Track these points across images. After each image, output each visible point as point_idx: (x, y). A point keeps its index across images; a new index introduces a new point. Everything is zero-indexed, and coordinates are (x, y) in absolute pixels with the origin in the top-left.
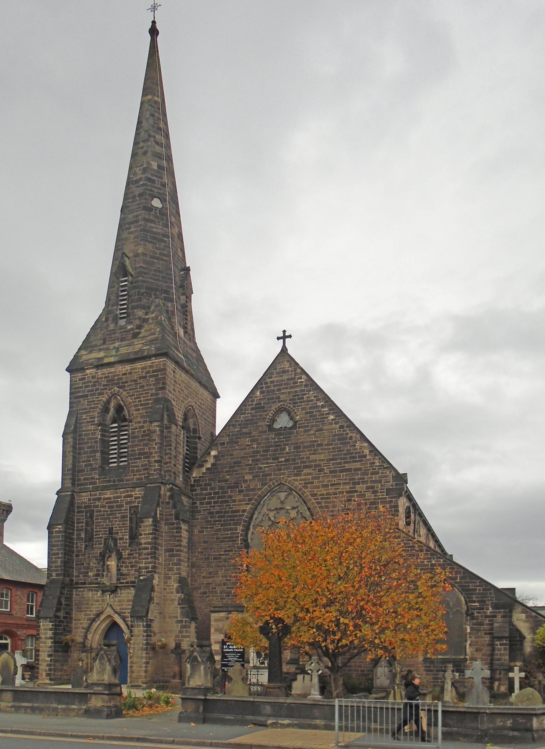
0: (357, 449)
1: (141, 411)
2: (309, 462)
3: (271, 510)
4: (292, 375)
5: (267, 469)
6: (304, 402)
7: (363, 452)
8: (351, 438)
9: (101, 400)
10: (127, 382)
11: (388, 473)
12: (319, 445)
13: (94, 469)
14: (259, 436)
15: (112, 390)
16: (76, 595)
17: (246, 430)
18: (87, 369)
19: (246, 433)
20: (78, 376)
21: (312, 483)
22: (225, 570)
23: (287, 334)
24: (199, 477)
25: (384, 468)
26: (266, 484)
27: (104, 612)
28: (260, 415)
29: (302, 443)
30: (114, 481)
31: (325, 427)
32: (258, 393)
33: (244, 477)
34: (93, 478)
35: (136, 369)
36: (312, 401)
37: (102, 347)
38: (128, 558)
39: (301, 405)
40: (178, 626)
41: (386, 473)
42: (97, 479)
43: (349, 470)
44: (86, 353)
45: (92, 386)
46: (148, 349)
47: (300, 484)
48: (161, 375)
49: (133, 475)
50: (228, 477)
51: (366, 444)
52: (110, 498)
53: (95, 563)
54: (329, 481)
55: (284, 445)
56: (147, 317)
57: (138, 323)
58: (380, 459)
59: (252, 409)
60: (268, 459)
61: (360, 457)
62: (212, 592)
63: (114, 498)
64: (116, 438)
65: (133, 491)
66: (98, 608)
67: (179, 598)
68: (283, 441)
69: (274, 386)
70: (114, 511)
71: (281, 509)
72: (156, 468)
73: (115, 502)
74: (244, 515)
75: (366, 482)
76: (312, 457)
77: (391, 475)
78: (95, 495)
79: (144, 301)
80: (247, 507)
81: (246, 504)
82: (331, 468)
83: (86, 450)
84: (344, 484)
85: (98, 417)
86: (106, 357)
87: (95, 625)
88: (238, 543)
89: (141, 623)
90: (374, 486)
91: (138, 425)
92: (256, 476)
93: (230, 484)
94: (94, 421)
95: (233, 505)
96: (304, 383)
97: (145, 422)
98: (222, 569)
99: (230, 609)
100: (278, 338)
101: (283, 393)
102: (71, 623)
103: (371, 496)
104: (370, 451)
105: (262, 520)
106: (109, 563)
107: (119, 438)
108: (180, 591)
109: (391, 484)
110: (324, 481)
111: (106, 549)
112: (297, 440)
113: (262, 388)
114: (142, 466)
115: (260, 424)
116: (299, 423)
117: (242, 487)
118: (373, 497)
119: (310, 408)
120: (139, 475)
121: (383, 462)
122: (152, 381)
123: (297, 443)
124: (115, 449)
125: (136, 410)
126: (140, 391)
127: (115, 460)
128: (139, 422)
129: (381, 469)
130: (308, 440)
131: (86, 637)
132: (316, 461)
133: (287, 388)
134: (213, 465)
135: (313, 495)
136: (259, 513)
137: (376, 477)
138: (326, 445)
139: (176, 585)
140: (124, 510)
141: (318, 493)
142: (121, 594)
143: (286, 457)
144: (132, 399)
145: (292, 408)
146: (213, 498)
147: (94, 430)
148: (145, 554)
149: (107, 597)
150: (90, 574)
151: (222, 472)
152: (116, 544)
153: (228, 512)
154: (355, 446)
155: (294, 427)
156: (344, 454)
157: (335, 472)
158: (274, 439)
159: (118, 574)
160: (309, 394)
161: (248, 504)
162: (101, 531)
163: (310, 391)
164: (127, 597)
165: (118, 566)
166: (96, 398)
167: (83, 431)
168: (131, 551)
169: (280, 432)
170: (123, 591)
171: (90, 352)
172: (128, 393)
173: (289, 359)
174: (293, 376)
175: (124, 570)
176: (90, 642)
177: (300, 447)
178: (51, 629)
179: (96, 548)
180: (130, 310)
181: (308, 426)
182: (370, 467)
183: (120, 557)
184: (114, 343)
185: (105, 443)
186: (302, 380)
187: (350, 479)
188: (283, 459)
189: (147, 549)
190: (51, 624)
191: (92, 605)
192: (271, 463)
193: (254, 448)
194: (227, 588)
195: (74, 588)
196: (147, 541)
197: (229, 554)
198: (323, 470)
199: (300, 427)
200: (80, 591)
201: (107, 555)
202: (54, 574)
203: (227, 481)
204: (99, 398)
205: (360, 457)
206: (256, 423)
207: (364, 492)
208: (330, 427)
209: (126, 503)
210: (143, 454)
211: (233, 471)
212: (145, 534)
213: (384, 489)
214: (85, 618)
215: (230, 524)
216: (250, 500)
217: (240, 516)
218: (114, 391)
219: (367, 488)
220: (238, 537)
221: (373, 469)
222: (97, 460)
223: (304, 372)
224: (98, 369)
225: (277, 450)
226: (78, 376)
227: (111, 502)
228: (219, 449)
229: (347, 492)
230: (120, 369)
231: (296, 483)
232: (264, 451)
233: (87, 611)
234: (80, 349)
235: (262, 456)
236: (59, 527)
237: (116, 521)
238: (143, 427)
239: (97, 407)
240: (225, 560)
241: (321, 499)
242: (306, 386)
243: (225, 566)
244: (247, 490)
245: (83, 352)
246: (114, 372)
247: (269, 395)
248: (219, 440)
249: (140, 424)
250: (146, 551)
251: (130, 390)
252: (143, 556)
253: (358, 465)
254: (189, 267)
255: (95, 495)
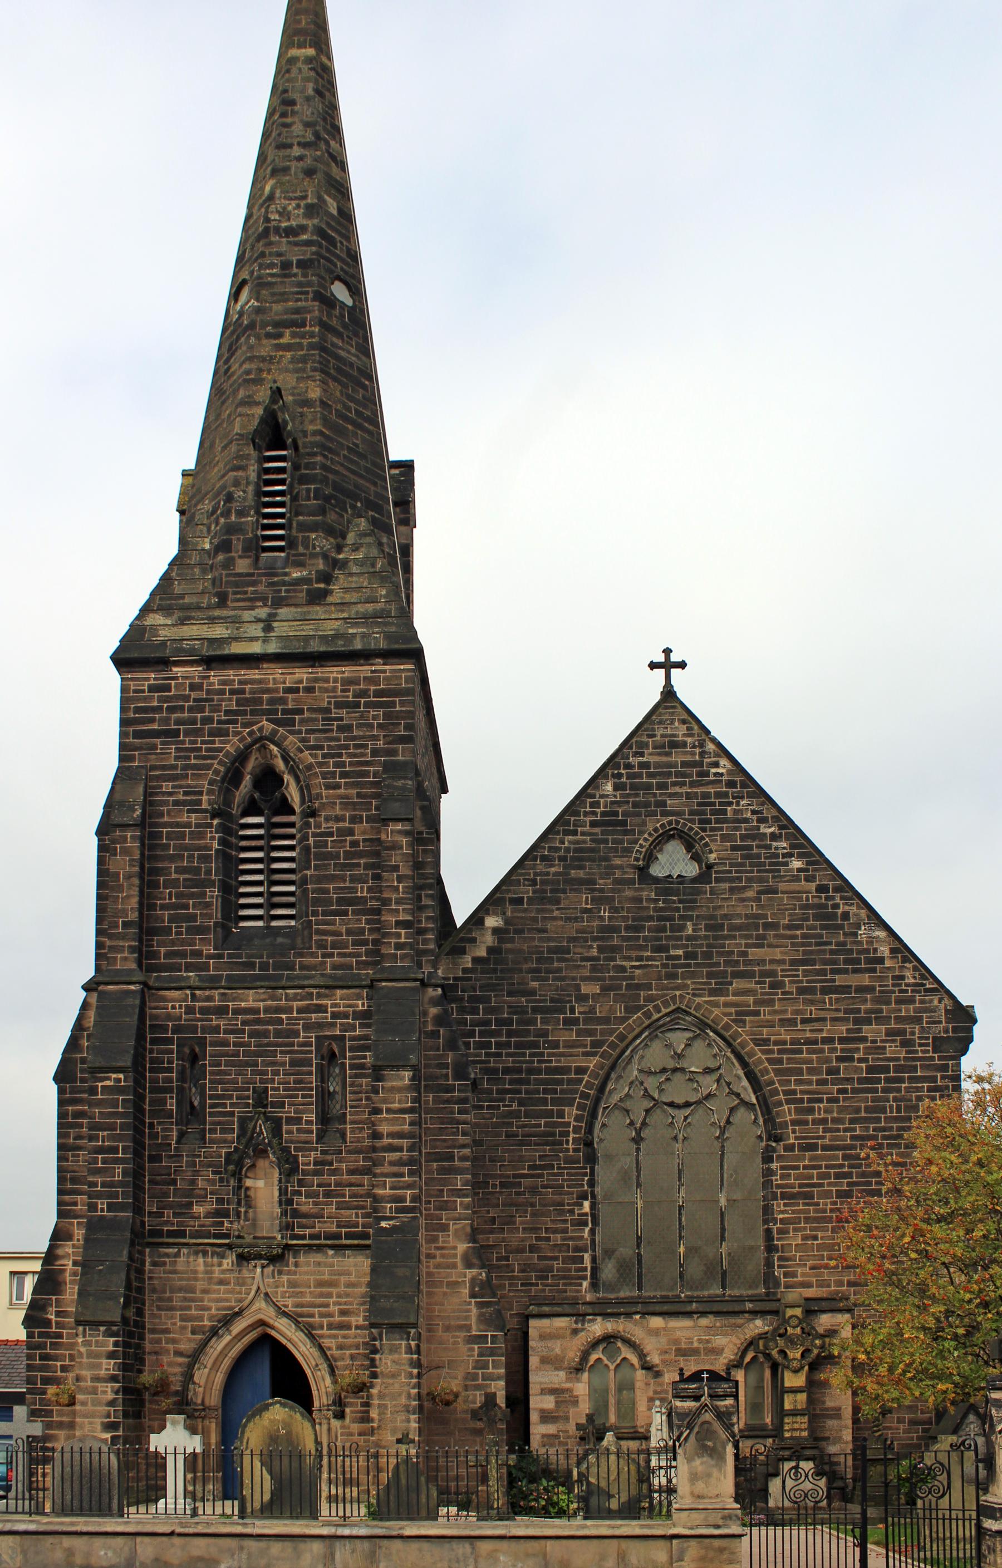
0: (860, 943)
1: (342, 791)
2: (747, 963)
3: (650, 1073)
4: (693, 754)
5: (638, 972)
6: (725, 821)
7: (875, 950)
8: (846, 916)
9: (220, 750)
10: (300, 711)
11: (936, 1002)
12: (767, 926)
13: (202, 930)
14: (613, 890)
15: (254, 728)
16: (154, 1264)
17: (581, 874)
18: (177, 664)
19: (581, 882)
20: (148, 679)
21: (757, 1013)
22: (533, 1215)
23: (674, 658)
24: (455, 979)
25: (926, 990)
26: (639, 1008)
27: (246, 1313)
28: (614, 841)
29: (725, 917)
30: (264, 966)
31: (782, 886)
32: (609, 787)
33: (578, 988)
34: (198, 954)
35: (327, 680)
36: (746, 821)
37: (217, 613)
38: (316, 1173)
39: (721, 829)
40: (472, 1349)
41: (931, 1001)
42: (210, 957)
43: (845, 989)
44: (169, 622)
45: (191, 709)
46: (364, 636)
47: (725, 1014)
48: (402, 704)
49: (324, 956)
50: (535, 984)
51: (882, 934)
52: (256, 1011)
53: (212, 1182)
54: (797, 1012)
55: (682, 918)
56: (341, 556)
57: (321, 567)
58: (915, 969)
59: (593, 824)
60: (641, 948)
61: (868, 961)
62: (499, 1267)
63: (267, 1010)
64: (260, 855)
65: (326, 996)
66: (227, 1300)
67: (473, 1281)
68: (678, 909)
69: (651, 775)
70: (268, 1045)
71: (675, 1070)
72: (403, 940)
73: (271, 1021)
74: (581, 1080)
75: (887, 1020)
76: (754, 953)
77: (942, 1006)
78: (209, 999)
79: (331, 517)
80: (590, 1062)
81: (586, 1054)
82: (801, 982)
83: (174, 876)
84: (834, 1020)
85: (210, 792)
86: (236, 639)
87: (218, 1345)
88: (568, 1150)
89: (404, 1343)
90: (905, 1030)
91: (335, 826)
92: (610, 988)
93: (539, 1001)
94: (199, 802)
95: (549, 1054)
96: (724, 778)
97: (354, 819)
98: (526, 1211)
99: (582, 1309)
100: (653, 666)
101: (672, 795)
102: (142, 1337)
103: (899, 1052)
104: (893, 951)
105: (627, 1095)
106: (249, 1183)
107: (268, 854)
108: (475, 1261)
109: (943, 1027)
110: (785, 1011)
111: (247, 1146)
112: (715, 908)
113: (619, 776)
114: (349, 932)
115: (617, 862)
116: (716, 868)
117: (572, 1011)
118: (903, 1055)
119: (743, 837)
120: (341, 955)
121: (923, 977)
122: (375, 718)
123: (712, 917)
124: (259, 883)
125: (328, 787)
126: (338, 739)
127: (260, 912)
128: (338, 819)
129: (919, 992)
130: (740, 910)
131: (188, 1377)
132: (761, 962)
133: (682, 784)
134: (490, 950)
135: (758, 1042)
136: (620, 1077)
137: (907, 1010)
138: (788, 927)
139: (462, 1247)
140: (300, 1045)
141: (773, 1038)
142: (296, 1265)
143: (687, 946)
144: (315, 756)
145: (697, 834)
146: (497, 1033)
147: (197, 826)
148: (392, 1163)
149: (257, 1274)
150: (198, 1209)
151: (521, 971)
152: (276, 1131)
153: (539, 1071)
154: (855, 935)
155: (703, 877)
156: (832, 952)
157: (811, 991)
158: (656, 901)
159: (284, 1213)
160: (738, 804)
161: (594, 1054)
162: (231, 1097)
163: (742, 798)
164: (314, 1273)
165: (283, 1191)
166: (203, 742)
167: (165, 825)
168: (323, 1152)
169: (668, 885)
170: (302, 1259)
171: (182, 622)
172: (303, 740)
173: (685, 716)
174: (697, 758)
175: (305, 1204)
176: (201, 1390)
177: (721, 927)
178: (111, 1355)
179: (212, 1141)
180: (294, 532)
181: (740, 879)
182: (893, 985)
183: (289, 1167)
184: (252, 608)
185: (230, 864)
186: (720, 770)
187: (847, 1011)
188: (680, 952)
189: (400, 1149)
190: (112, 1339)
191: (205, 1291)
192: (649, 958)
193: (602, 918)
194: (540, 1258)
195: (149, 1245)
196: (397, 1128)
197: (541, 1176)
198: (780, 985)
199: (718, 880)
200: (167, 1255)
201: (248, 1162)
202: (102, 1204)
203: (532, 993)
204: (214, 742)
205: (868, 961)
206: (607, 859)
207: (882, 1041)
208: (794, 886)
209: (307, 1027)
210: (351, 902)
211: (548, 971)
212: (389, 1111)
213: (928, 1038)
214: (183, 1328)
215: (544, 1102)
216: (596, 1044)
217: (570, 1081)
218: (261, 729)
219: (889, 1033)
220: (567, 1134)
221: (901, 991)
222: (208, 905)
223: (723, 751)
224: (209, 669)
225: (663, 929)
226: (148, 679)
227: (258, 1021)
228: (509, 914)
229: (842, 1040)
230: (277, 676)
231: (716, 1011)
232: (628, 928)
233: (189, 1308)
234: (146, 610)
235: (624, 939)
236: (114, 1076)
237: (276, 1073)
238: (351, 832)
239: (209, 767)
240: (533, 1190)
241: (780, 1051)
242: (731, 784)
243: (533, 1205)
244: (586, 1021)
245: (156, 619)
246: (260, 682)
247: (637, 795)
248: (508, 891)
249: (341, 825)
250: (395, 1156)
251: (308, 732)
252: (387, 1169)
253: (865, 979)
254: (407, 467)
255: (209, 999)
